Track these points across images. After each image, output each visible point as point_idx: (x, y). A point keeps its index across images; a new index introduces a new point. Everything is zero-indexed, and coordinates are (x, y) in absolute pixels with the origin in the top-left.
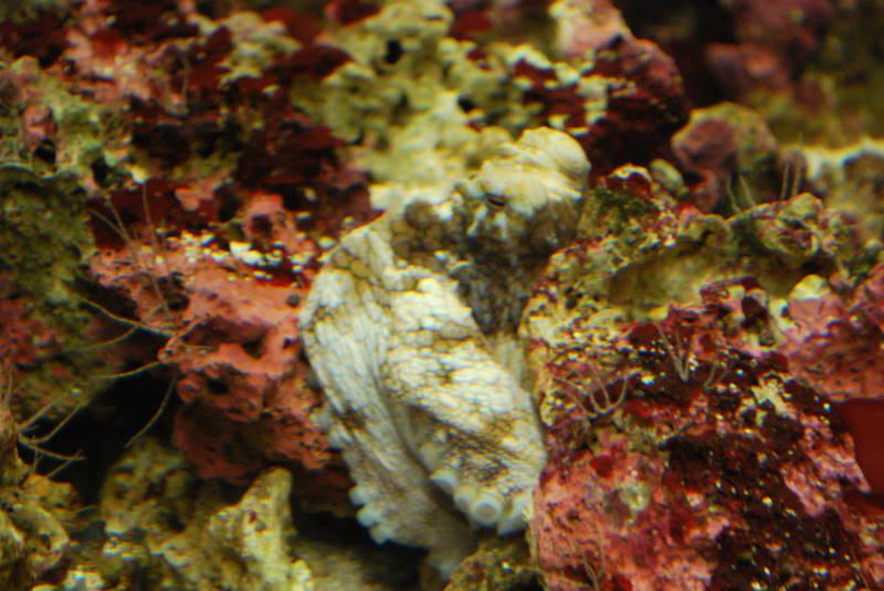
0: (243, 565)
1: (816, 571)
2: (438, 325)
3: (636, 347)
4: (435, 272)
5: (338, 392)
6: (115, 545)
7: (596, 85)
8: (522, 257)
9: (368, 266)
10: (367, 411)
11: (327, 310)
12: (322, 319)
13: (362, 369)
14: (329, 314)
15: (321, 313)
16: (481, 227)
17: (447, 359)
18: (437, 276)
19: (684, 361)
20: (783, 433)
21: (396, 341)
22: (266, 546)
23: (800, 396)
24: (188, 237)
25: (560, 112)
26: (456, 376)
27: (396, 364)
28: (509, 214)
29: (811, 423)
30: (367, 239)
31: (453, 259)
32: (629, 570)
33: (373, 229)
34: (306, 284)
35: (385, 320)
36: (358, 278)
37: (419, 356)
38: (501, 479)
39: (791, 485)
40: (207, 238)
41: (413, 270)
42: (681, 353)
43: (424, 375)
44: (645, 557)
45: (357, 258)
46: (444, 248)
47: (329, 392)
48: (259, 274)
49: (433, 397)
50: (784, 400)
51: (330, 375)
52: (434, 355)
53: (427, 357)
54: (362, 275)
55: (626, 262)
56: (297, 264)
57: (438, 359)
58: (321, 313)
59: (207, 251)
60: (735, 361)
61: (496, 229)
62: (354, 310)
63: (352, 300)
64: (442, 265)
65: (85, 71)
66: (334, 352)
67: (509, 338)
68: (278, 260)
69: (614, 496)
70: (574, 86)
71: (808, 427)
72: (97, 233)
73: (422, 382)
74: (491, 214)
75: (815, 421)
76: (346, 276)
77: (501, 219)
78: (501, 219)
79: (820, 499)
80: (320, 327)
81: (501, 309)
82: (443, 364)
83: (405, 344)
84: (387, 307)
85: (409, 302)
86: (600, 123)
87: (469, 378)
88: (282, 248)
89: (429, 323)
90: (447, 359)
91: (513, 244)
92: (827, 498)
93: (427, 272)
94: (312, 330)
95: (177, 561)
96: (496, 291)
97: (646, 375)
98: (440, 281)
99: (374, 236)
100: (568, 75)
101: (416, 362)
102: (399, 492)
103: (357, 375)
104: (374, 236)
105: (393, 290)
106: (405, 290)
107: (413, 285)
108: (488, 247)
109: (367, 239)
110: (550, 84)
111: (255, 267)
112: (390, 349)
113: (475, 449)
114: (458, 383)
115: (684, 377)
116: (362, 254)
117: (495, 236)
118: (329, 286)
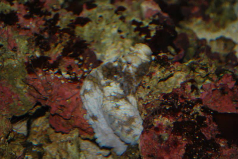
0: (68, 153)
1: (209, 153)
2: (115, 95)
3: (165, 99)
4: (114, 81)
5: (91, 111)
6: (35, 148)
7: (153, 27)
8: (136, 76)
9: (97, 79)
10: (98, 116)
11: (87, 91)
12: (86, 93)
13: (96, 105)
14: (88, 92)
15: (86, 91)
16: (125, 70)
17: (118, 103)
18: (114, 82)
19: (177, 102)
20: (201, 120)
21: (105, 99)
22: (73, 149)
23: (205, 110)
24: (51, 71)
25: (144, 34)
26: (121, 107)
27: (105, 105)
28: (132, 66)
29: (208, 117)
30: (96, 72)
31: (119, 77)
32: (163, 155)
33: (98, 69)
34: (81, 83)
35: (102, 94)
36: (94, 83)
37: (110, 103)
38: (132, 133)
39: (203, 133)
40: (56, 71)
41: (108, 80)
42: (176, 101)
43: (112, 107)
44: (168, 151)
45: (94, 77)
46: (116, 74)
47: (88, 111)
48: (69, 81)
49: (114, 113)
50: (202, 111)
51: (89, 107)
52: (115, 102)
53: (113, 103)
54: (96, 82)
55: (148, 115)
56: (79, 78)
57: (116, 103)
58: (86, 91)
59: (56, 75)
60: (186, 104)
61: (129, 70)
62: (94, 91)
63: (93, 88)
64: (116, 79)
65: (22, 27)
66: (89, 102)
67: (132, 96)
68: (74, 77)
69: (160, 137)
70: (147, 27)
71: (207, 118)
72: (28, 70)
73: (112, 109)
74: (128, 67)
75: (209, 116)
76: (92, 82)
77: (130, 68)
78: (130, 68)
79: (210, 136)
80: (86, 95)
81: (131, 89)
82: (117, 105)
83: (107, 100)
84: (102, 90)
85: (108, 89)
86: (154, 36)
87: (123, 108)
88: (75, 73)
89: (113, 94)
90: (118, 103)
91: (134, 73)
92: (212, 135)
93: (112, 81)
94: (83, 95)
95: (51, 151)
96: (129, 85)
97: (167, 107)
98: (115, 83)
99: (98, 71)
100: (146, 24)
101: (110, 104)
102: (106, 135)
103: (95, 108)
104: (98, 71)
105: (103, 86)
106: (107, 86)
107: (108, 84)
108: (127, 74)
109: (96, 72)
110: (142, 26)
111: (68, 79)
112: (103, 101)
113: (125, 125)
114: (121, 109)
115: (177, 107)
116: (96, 76)
117: (129, 72)
118: (87, 85)
